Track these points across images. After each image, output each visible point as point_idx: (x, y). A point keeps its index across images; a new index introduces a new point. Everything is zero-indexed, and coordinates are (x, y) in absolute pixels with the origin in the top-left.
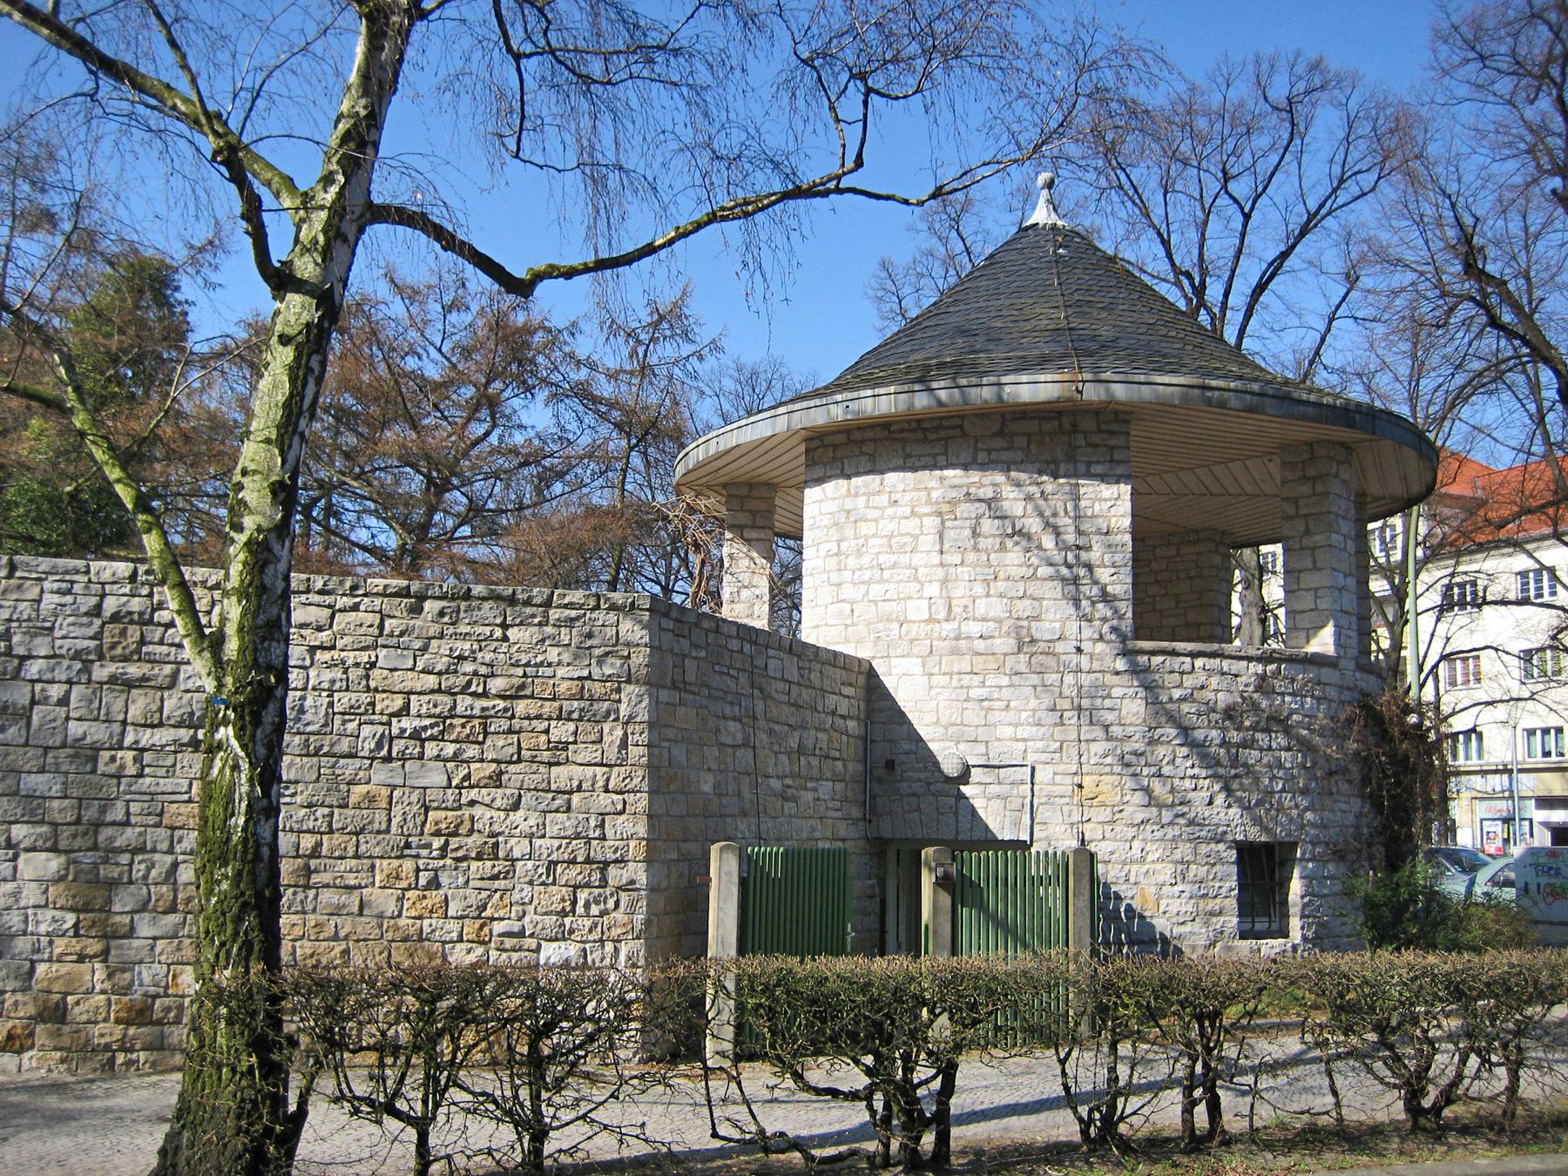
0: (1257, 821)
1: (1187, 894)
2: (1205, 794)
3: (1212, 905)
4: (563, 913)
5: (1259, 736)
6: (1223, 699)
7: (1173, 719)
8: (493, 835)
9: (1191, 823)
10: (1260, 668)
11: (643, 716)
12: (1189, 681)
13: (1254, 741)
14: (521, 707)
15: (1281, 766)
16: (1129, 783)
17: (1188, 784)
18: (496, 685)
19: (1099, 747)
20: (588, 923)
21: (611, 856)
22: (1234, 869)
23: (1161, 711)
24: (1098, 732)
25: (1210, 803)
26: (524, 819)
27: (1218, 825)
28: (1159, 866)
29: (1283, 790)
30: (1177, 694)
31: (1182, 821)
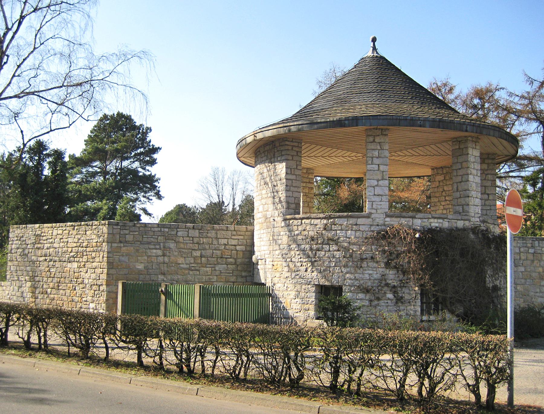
0: (325, 277)
1: (298, 303)
2: (305, 268)
3: (306, 307)
4: (93, 297)
5: (324, 246)
6: (311, 233)
7: (295, 241)
8: (83, 279)
9: (300, 277)
10: (325, 221)
11: (106, 250)
12: (300, 228)
13: (323, 248)
14: (88, 249)
15: (334, 257)
16: (285, 264)
17: (299, 264)
18: (84, 244)
19: (277, 252)
20: (96, 299)
21: (100, 284)
22: (314, 294)
23: (293, 239)
24: (277, 247)
25: (306, 271)
26: (87, 275)
27: (308, 279)
28: (291, 292)
29: (335, 266)
30: (296, 232)
31: (298, 277)
